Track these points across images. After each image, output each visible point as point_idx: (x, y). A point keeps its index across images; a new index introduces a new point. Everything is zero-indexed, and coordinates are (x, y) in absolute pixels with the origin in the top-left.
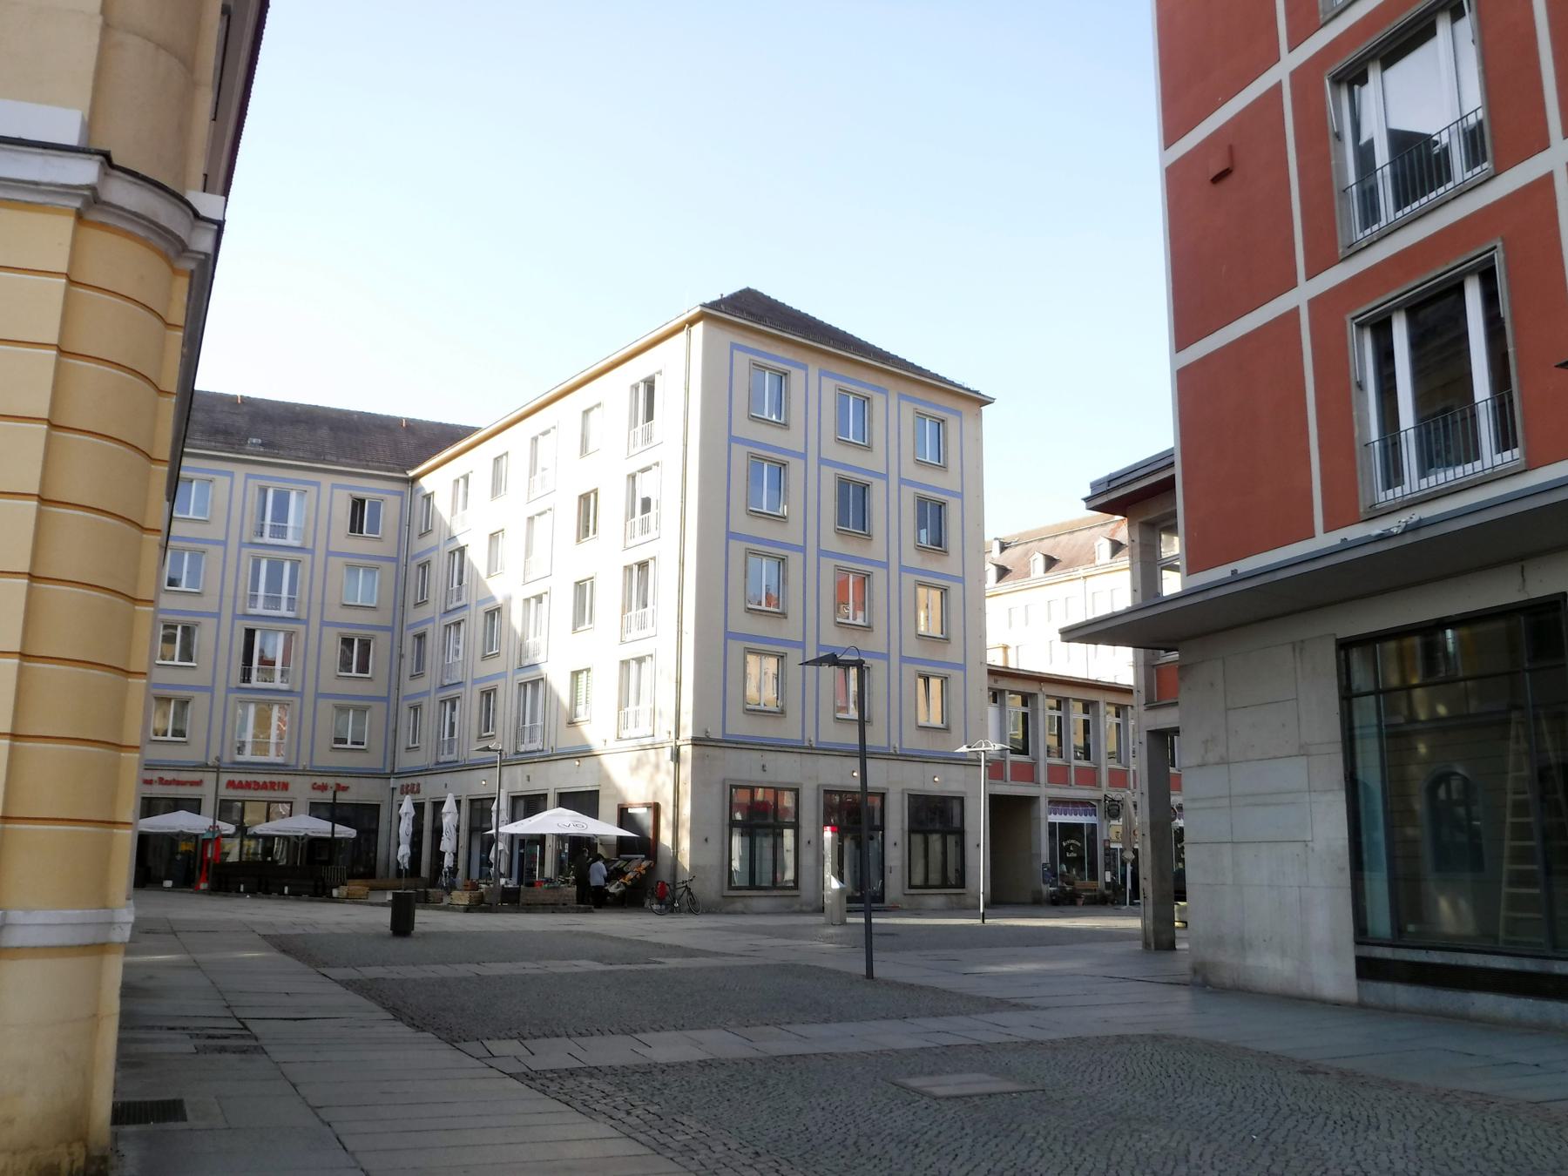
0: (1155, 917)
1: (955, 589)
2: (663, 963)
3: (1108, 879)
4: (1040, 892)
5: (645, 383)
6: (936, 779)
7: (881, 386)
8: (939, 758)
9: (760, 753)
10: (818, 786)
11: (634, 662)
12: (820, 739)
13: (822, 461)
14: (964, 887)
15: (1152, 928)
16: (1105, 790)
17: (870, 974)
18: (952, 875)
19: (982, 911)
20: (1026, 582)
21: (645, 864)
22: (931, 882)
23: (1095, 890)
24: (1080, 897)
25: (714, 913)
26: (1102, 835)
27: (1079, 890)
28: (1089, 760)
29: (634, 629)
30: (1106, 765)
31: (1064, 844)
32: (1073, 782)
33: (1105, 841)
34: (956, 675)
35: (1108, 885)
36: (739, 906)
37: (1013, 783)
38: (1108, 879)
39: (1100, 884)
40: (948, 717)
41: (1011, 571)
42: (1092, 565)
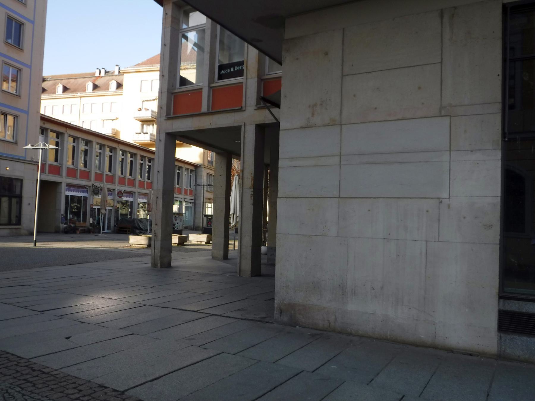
0: (161, 248)
3: (91, 222)
4: (59, 227)
6: (8, 169)
8: (10, 158)
15: (159, 254)
16: (93, 182)
18: (14, 220)
19: (34, 239)
20: (53, 96)
23: (85, 226)
26: (89, 202)
28: (86, 168)
30: (94, 170)
31: (72, 205)
32: (78, 177)
33: (91, 205)
34: (23, 117)
38: (91, 222)
39: (87, 224)
40: (16, 137)
41: (47, 90)
42: (84, 92)
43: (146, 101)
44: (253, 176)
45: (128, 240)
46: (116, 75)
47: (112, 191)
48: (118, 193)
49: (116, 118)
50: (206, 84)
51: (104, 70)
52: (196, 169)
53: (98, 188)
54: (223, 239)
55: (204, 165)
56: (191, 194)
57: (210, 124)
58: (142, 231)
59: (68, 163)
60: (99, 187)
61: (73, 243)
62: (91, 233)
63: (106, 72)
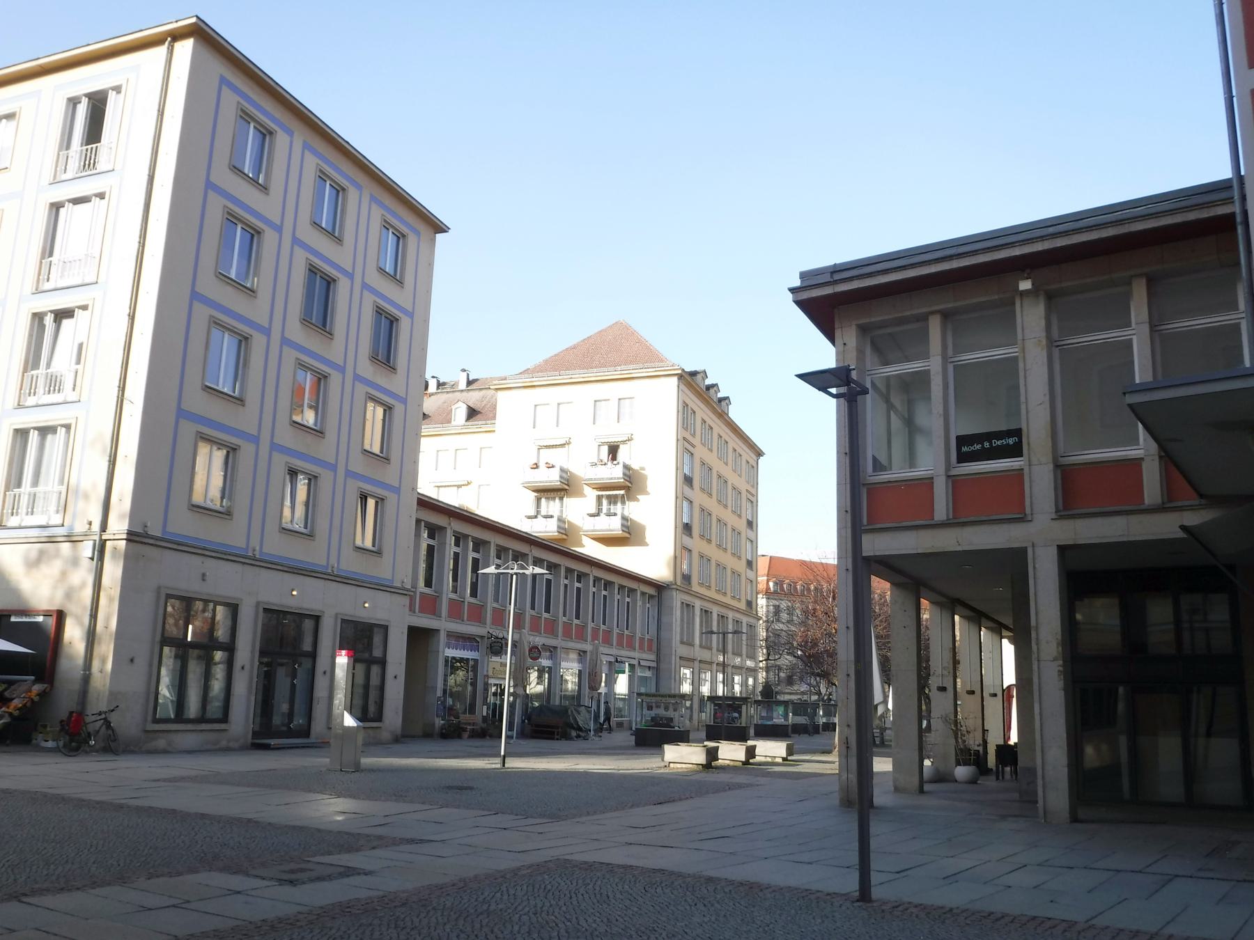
1: (399, 408)
2: (349, 872)
5: (89, 99)
7: (356, 180)
9: (201, 559)
10: (258, 603)
11: (36, 432)
12: (265, 550)
13: (296, 241)
14: (381, 721)
17: (865, 893)
19: (502, 753)
21: (37, 688)
22: (209, 715)
24: (466, 731)
25: (132, 752)
27: (463, 723)
29: (40, 390)
35: (485, 719)
36: (161, 743)
37: (420, 615)
43: (547, 447)
44: (1059, 637)
45: (662, 754)
46: (462, 391)
47: (478, 639)
48: (530, 650)
49: (467, 483)
50: (941, 470)
51: (435, 380)
52: (658, 594)
53: (500, 640)
54: (917, 751)
55: (676, 584)
56: (650, 649)
57: (957, 544)
58: (580, 733)
59: (447, 593)
60: (502, 639)
61: (523, 759)
62: (488, 737)
63: (440, 385)
